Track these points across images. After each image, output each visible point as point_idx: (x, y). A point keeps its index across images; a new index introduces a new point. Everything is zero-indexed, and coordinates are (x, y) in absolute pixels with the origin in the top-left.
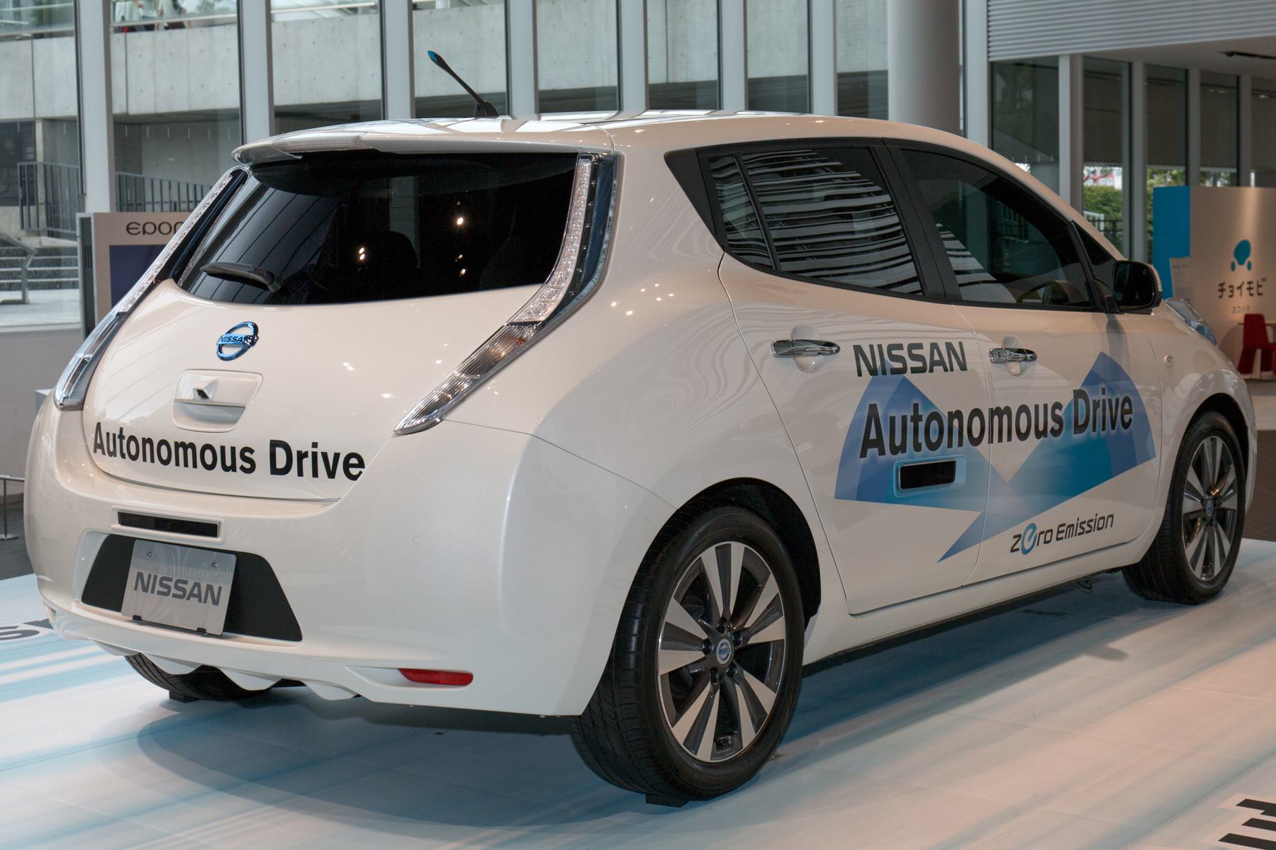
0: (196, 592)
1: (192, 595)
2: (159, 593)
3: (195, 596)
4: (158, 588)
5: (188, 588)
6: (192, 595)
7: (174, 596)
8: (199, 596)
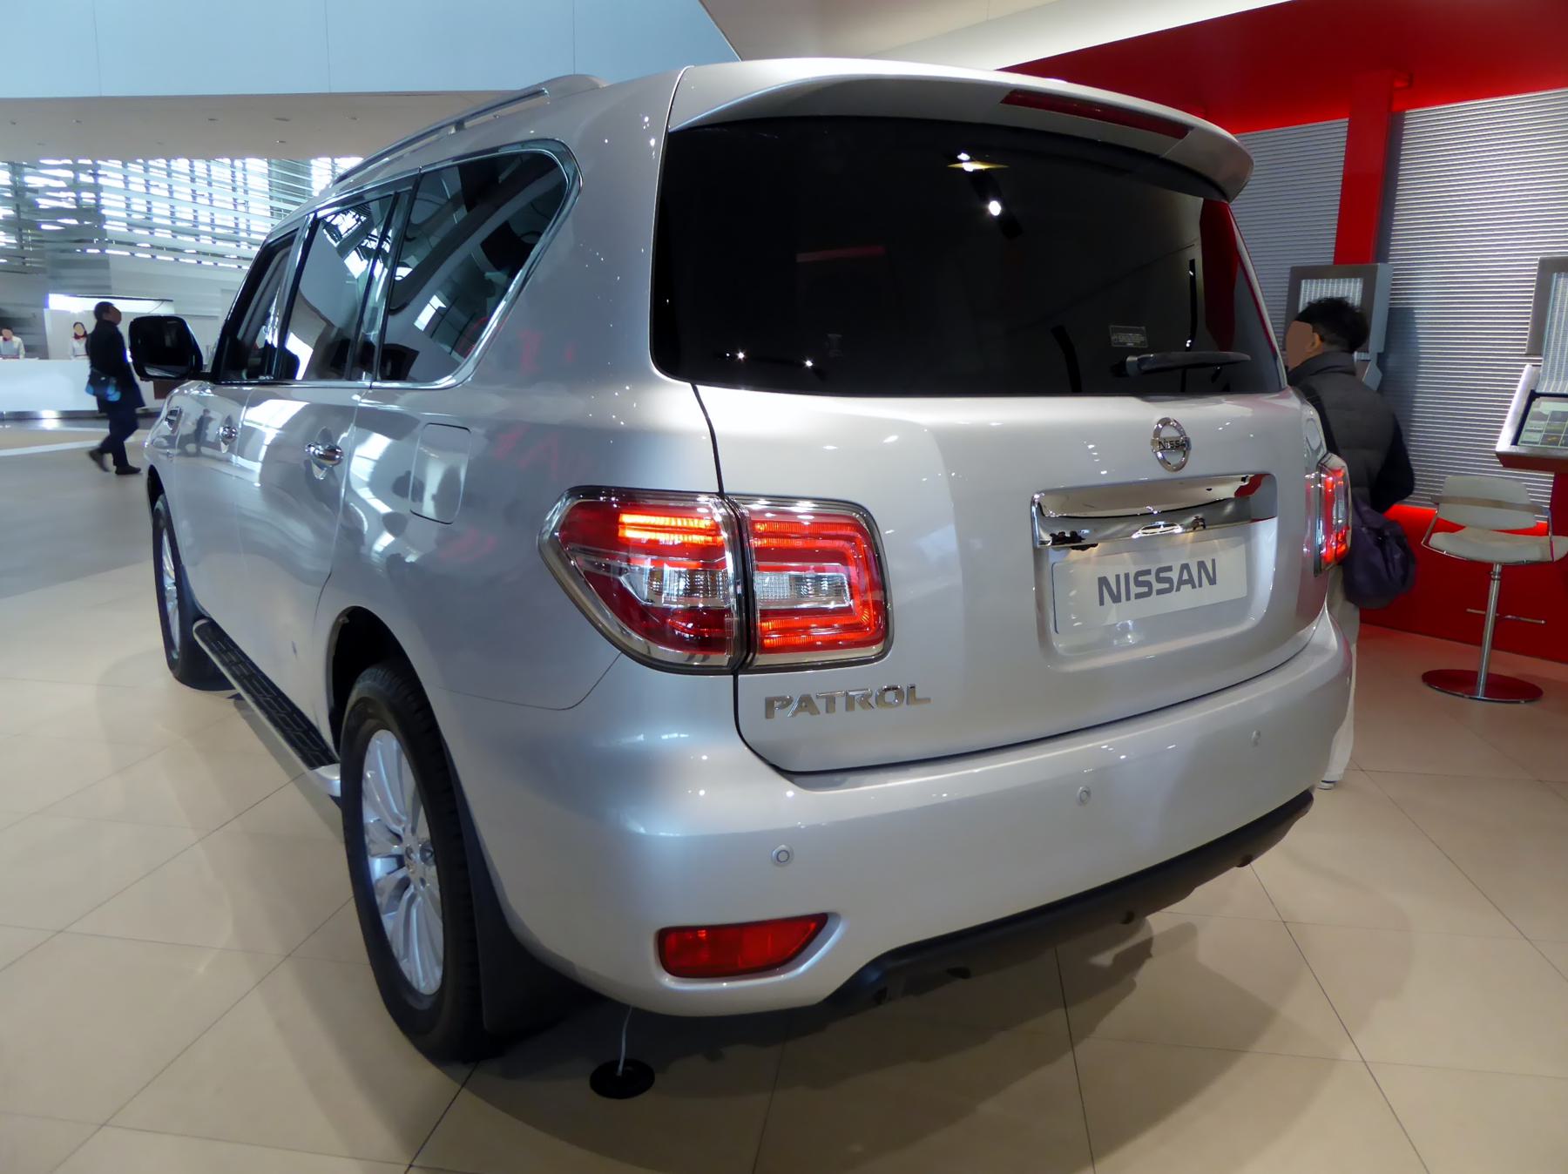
0: (1186, 577)
1: (1181, 582)
2: (1138, 596)
3: (1186, 582)
4: (1134, 590)
5: (1174, 575)
6: (1181, 582)
7: (1160, 592)
8: (1190, 581)
